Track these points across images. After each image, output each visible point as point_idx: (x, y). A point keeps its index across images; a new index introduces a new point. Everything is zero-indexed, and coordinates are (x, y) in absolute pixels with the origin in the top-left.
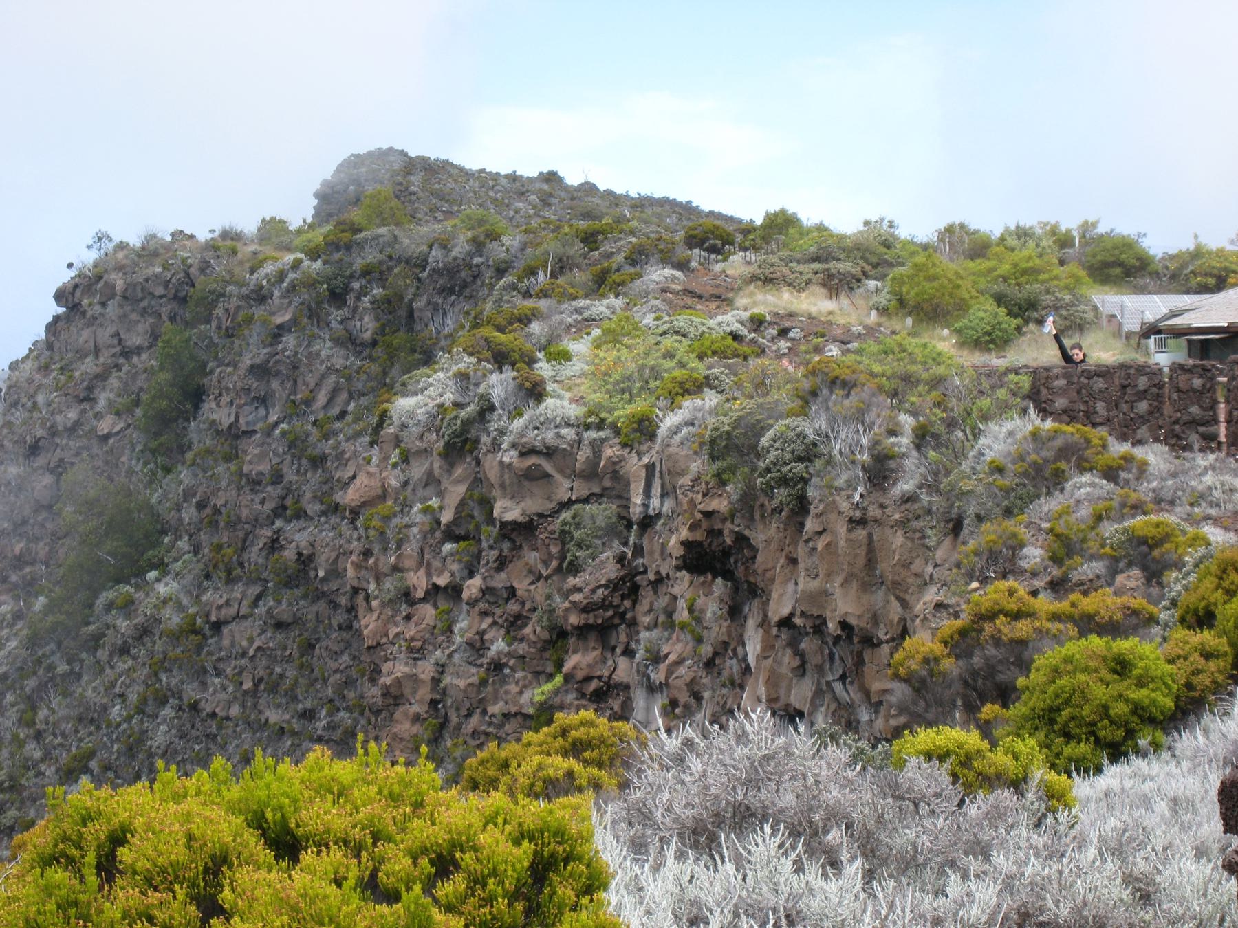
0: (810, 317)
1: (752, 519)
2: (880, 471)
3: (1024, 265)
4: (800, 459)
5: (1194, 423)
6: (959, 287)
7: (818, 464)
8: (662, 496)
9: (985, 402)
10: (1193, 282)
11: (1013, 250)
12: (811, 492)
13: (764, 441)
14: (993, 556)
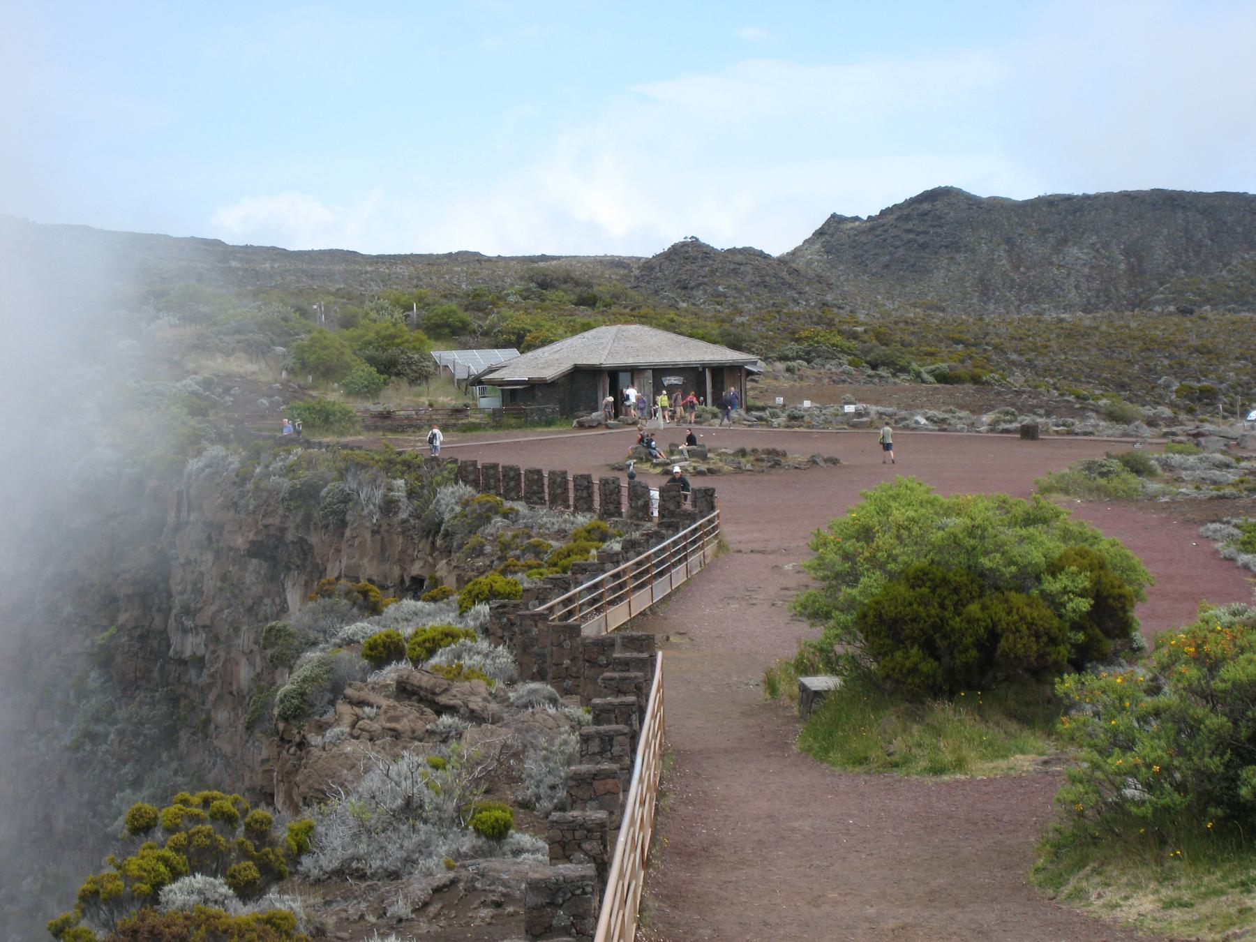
0: (241, 376)
1: (309, 529)
2: (389, 507)
3: (383, 333)
4: (342, 502)
5: (535, 493)
6: (342, 353)
7: (351, 504)
8: (189, 511)
9: (439, 478)
10: (502, 338)
11: (375, 321)
12: (349, 518)
13: (323, 493)
14: (474, 549)
